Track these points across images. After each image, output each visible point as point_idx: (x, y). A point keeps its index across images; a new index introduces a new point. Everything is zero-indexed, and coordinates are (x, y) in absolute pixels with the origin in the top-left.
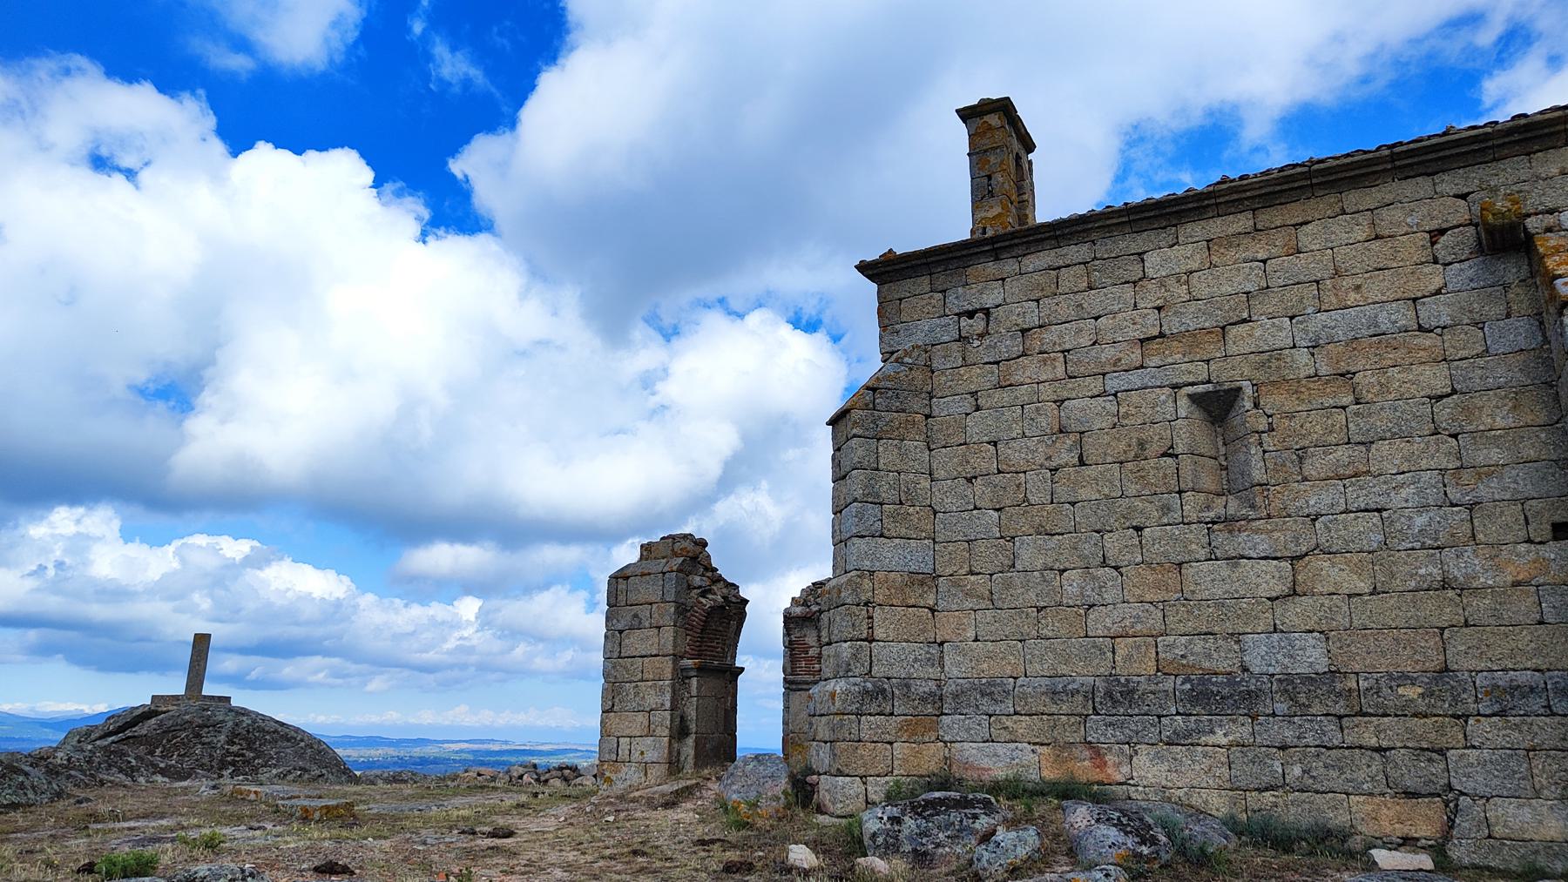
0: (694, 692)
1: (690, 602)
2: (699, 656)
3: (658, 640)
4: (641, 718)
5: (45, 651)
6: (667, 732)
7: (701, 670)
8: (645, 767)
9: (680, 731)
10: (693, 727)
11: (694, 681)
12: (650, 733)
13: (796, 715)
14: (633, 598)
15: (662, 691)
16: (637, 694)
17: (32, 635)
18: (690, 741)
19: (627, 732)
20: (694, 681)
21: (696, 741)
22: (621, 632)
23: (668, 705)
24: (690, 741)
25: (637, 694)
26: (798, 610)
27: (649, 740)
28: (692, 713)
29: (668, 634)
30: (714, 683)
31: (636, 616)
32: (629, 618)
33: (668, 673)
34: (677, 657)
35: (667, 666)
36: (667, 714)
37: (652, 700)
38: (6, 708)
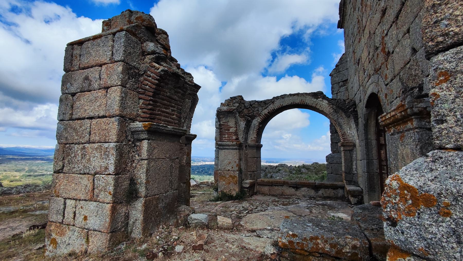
0: (145, 154)
1: (143, 67)
2: (151, 119)
3: (107, 101)
4: (86, 181)
5: (41, 135)
6: (109, 198)
7: (153, 133)
8: (87, 234)
9: (126, 194)
10: (142, 190)
11: (145, 144)
12: (93, 198)
13: (223, 161)
14: (85, 61)
15: (106, 153)
16: (83, 156)
17: (37, 132)
18: (139, 205)
19: (73, 194)
20: (145, 144)
21: (146, 206)
22: (73, 95)
23: (112, 169)
24: (139, 205)
25: (83, 156)
26: (225, 108)
27: (92, 205)
28: (141, 176)
29: (115, 94)
30: (166, 147)
31: (87, 78)
32: (80, 80)
33: (113, 136)
34: (124, 119)
35: (113, 127)
36: (111, 179)
37: (96, 163)
38: (4, 145)
